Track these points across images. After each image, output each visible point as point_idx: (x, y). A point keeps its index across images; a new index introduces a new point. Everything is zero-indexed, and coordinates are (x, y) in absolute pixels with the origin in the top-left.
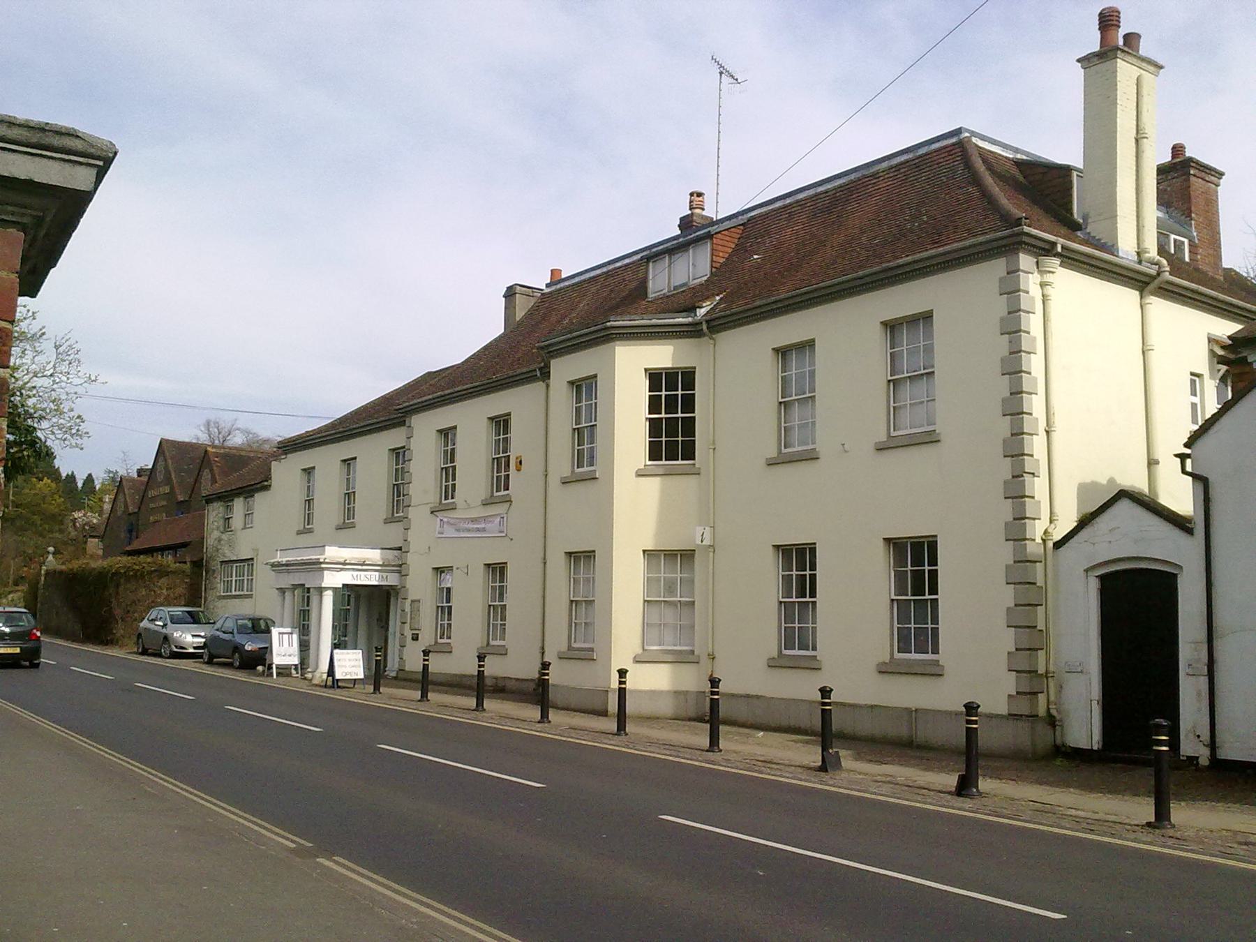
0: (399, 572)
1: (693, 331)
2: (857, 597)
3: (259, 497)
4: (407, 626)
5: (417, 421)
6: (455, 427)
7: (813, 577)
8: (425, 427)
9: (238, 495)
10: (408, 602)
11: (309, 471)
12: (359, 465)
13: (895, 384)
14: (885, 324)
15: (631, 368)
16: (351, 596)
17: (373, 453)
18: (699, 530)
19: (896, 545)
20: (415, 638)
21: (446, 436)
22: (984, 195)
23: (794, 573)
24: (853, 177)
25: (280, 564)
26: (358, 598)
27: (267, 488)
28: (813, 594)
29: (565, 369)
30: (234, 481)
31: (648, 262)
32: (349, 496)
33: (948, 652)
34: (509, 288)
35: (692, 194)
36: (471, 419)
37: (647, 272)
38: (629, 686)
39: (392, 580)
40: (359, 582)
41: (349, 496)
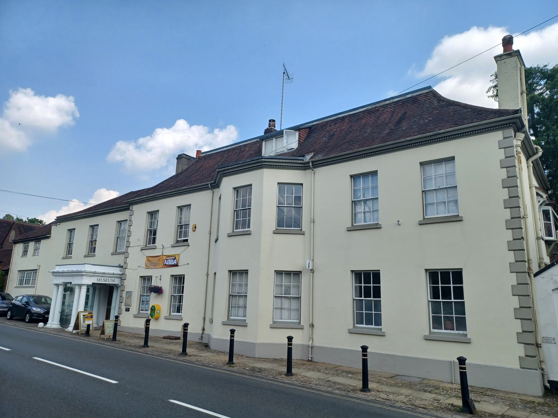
0: (121, 278)
1: (305, 167)
2: (406, 300)
3: (43, 242)
4: (123, 304)
5: (136, 208)
6: (75, 229)
7: (183, 287)
8: (140, 212)
9: (32, 240)
10: (124, 293)
11: (71, 231)
12: (100, 229)
13: (355, 203)
14: (351, 176)
15: (266, 185)
16: (95, 288)
17: (107, 224)
18: (308, 262)
19: (358, 275)
20: (128, 310)
21: (71, 232)
22: (463, 107)
23: (363, 285)
24: (369, 107)
25: (58, 272)
26: (100, 290)
27: (48, 238)
28: (183, 293)
29: (229, 184)
30: (30, 234)
31: (262, 140)
32: (70, 245)
33: (384, 327)
34: (180, 155)
35: (270, 121)
36: (167, 208)
37: (261, 146)
38: (236, 339)
39: (117, 281)
40: (100, 282)
41: (70, 245)
